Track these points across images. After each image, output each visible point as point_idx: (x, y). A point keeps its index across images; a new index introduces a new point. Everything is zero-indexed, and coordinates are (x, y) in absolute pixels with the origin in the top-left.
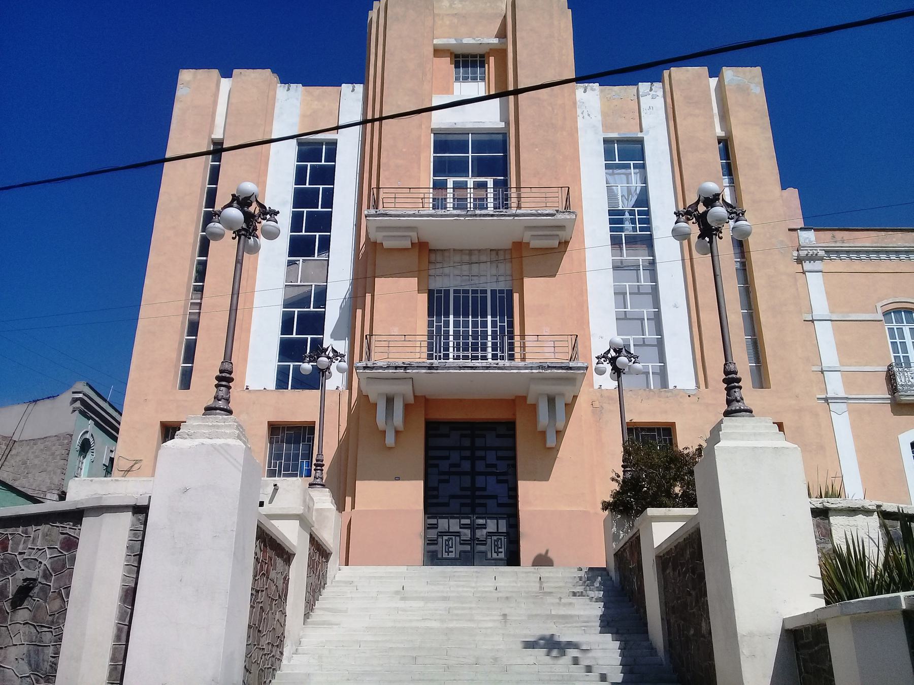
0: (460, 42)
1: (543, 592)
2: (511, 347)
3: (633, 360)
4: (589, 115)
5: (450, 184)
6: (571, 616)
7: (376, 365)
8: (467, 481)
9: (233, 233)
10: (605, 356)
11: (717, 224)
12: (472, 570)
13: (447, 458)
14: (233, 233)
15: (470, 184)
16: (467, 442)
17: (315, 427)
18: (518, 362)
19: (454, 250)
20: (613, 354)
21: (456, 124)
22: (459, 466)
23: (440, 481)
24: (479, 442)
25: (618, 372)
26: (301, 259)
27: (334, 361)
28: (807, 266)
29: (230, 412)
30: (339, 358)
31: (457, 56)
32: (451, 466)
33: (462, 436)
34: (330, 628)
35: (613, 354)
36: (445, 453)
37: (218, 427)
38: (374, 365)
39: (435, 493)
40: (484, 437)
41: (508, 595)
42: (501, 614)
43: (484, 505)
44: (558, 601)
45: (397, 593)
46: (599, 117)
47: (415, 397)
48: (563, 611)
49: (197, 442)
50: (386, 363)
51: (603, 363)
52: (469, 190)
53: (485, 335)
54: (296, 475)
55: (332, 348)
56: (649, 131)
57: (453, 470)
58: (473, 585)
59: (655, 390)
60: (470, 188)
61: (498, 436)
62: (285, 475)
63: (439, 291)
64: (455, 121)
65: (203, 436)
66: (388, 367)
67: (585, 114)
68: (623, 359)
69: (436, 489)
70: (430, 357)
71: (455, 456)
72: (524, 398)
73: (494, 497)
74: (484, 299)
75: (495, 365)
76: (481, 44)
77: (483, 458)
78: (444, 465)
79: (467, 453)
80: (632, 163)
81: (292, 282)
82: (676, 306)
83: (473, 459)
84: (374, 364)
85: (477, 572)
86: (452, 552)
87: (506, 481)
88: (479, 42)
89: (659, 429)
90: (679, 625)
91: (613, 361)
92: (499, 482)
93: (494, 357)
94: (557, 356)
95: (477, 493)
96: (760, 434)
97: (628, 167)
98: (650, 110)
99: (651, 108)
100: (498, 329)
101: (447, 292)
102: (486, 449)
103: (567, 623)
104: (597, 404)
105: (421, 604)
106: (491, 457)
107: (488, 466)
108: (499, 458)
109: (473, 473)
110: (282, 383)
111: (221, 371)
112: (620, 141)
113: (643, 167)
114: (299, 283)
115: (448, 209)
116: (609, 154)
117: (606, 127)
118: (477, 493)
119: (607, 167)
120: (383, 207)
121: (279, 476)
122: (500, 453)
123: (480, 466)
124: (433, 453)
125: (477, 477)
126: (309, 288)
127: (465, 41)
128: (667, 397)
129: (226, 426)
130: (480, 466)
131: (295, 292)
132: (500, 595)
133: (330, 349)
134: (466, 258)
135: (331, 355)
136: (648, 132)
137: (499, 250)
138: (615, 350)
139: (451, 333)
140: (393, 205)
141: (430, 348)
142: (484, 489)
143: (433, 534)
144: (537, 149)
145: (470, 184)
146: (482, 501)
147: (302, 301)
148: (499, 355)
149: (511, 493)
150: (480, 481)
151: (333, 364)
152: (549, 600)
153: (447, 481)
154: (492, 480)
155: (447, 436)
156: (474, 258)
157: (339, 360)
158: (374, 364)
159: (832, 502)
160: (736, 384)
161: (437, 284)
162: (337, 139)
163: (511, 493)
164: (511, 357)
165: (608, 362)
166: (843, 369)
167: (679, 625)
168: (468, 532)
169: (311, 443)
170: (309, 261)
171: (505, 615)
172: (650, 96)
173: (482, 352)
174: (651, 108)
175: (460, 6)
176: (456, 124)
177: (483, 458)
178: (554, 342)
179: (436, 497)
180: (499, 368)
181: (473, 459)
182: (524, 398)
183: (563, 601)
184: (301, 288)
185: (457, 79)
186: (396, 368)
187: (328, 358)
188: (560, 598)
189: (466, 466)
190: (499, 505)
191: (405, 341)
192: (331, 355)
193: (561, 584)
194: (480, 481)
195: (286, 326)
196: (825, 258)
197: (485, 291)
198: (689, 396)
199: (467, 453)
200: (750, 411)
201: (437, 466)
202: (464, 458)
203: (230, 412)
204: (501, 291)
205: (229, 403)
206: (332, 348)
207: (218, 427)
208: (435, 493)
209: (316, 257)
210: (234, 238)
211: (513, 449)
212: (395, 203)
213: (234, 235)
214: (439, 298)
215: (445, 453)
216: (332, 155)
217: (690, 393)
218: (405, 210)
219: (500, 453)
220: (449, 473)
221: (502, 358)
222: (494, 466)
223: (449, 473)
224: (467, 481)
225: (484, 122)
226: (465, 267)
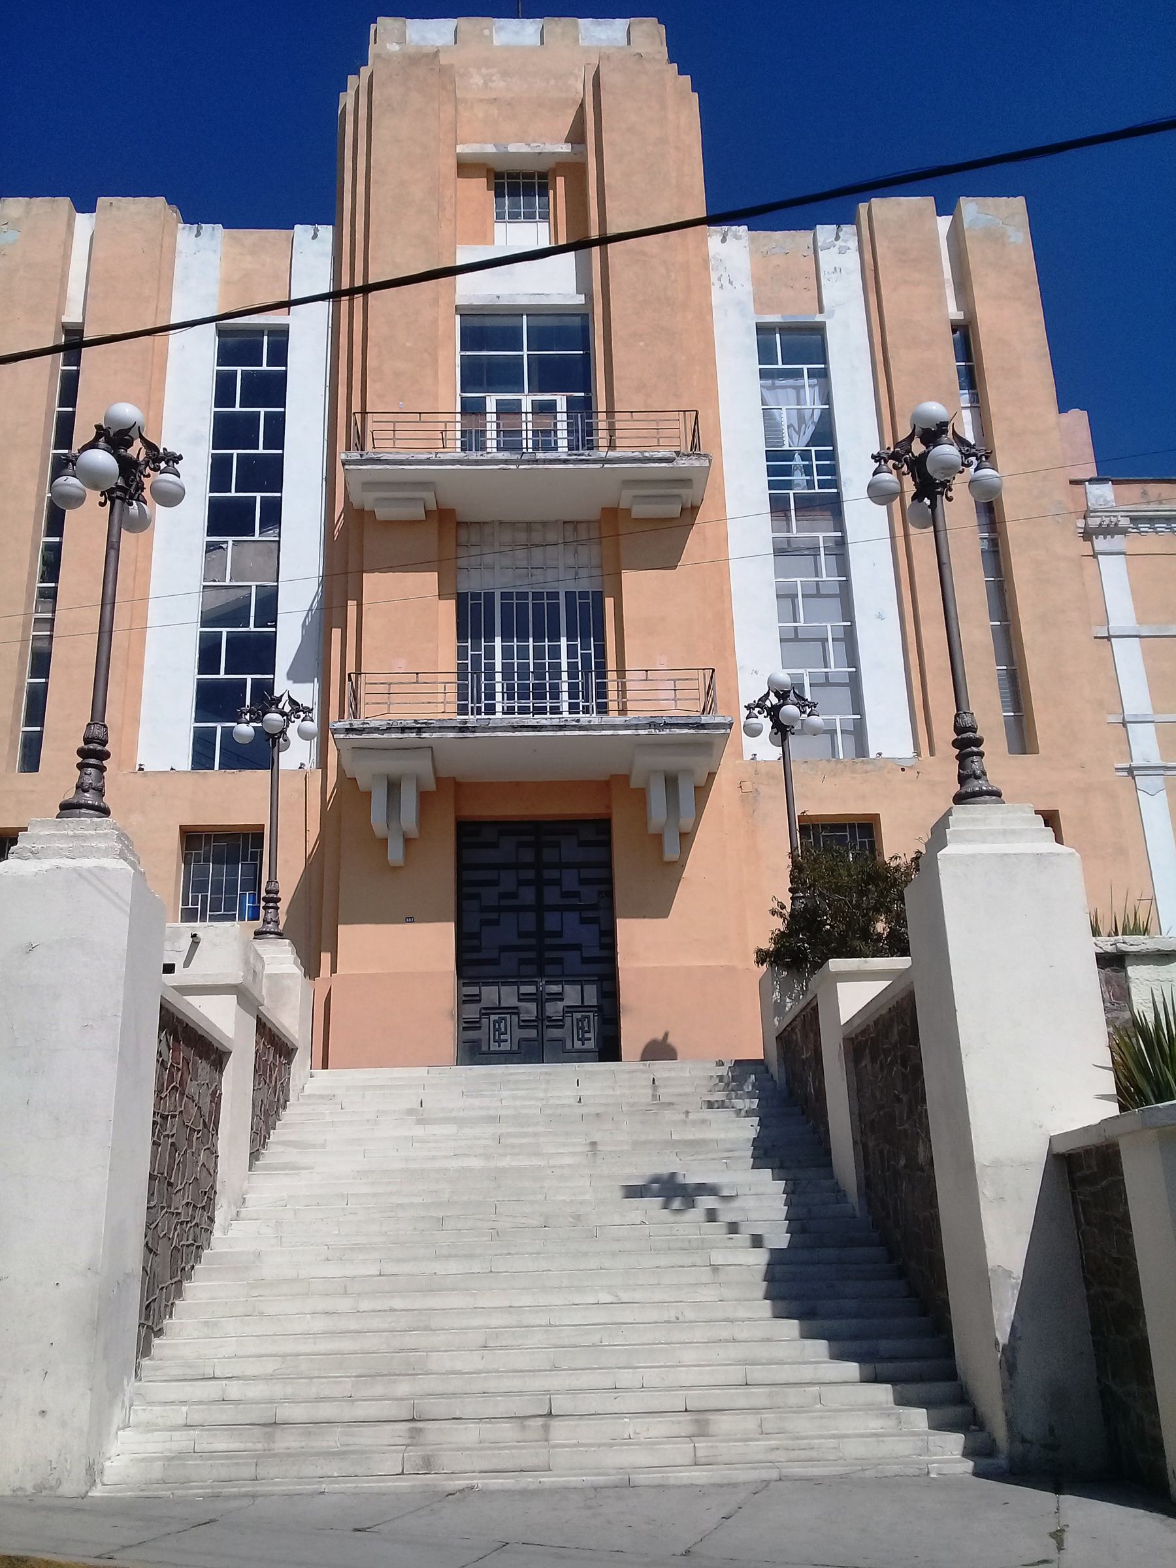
0: (502, 150)
1: (659, 1103)
2: (602, 691)
3: (808, 710)
4: (731, 283)
5: (491, 406)
6: (704, 1142)
7: (368, 726)
8: (529, 921)
9: (101, 495)
10: (760, 704)
11: (943, 475)
12: (539, 1071)
13: (495, 883)
14: (101, 495)
15: (527, 405)
16: (528, 856)
17: (263, 833)
18: (613, 717)
19: (501, 523)
20: (773, 700)
21: (498, 297)
22: (514, 895)
23: (484, 923)
24: (549, 855)
25: (782, 731)
26: (230, 539)
27: (293, 719)
28: (1101, 543)
29: (105, 812)
30: (301, 713)
31: (498, 175)
32: (504, 896)
33: (521, 845)
34: (296, 1174)
35: (773, 700)
36: (490, 875)
37: (84, 838)
38: (365, 726)
39: (475, 942)
40: (557, 845)
41: (600, 1110)
42: (588, 1141)
43: (559, 961)
44: (683, 1117)
45: (410, 1112)
46: (749, 287)
47: (438, 779)
48: (690, 1134)
49: (47, 864)
50: (385, 722)
51: (757, 717)
52: (524, 415)
53: (556, 671)
54: (232, 918)
55: (289, 696)
56: (834, 311)
57: (504, 902)
58: (541, 1095)
59: (846, 760)
60: (526, 413)
61: (583, 844)
62: (213, 918)
63: (476, 596)
64: (498, 293)
65: (58, 853)
66: (389, 729)
67: (725, 280)
68: (790, 710)
69: (477, 936)
70: (462, 710)
71: (508, 879)
72: (626, 778)
73: (577, 947)
74: (555, 608)
75: (574, 723)
76: (540, 153)
77: (557, 882)
78: (490, 895)
79: (530, 874)
80: (805, 367)
81: (214, 581)
82: (880, 617)
83: (539, 884)
84: (364, 723)
85: (546, 1073)
86: (506, 1041)
87: (595, 921)
88: (537, 151)
89: (852, 826)
90: (881, 1152)
91: (774, 713)
92: (583, 921)
93: (573, 709)
94: (680, 705)
95: (548, 941)
96: (1013, 832)
97: (798, 374)
98: (835, 275)
99: (838, 270)
100: (579, 660)
101: (490, 597)
102: (561, 866)
103: (697, 1153)
104: (748, 786)
105: (451, 1129)
106: (570, 880)
107: (565, 895)
108: (584, 882)
109: (540, 908)
110: (202, 758)
111: (87, 741)
112: (785, 329)
113: (823, 375)
114: (227, 583)
115: (489, 450)
116: (765, 353)
117: (761, 303)
118: (548, 941)
119: (763, 374)
120: (374, 448)
121: (203, 919)
122: (587, 873)
123: (552, 896)
124: (469, 875)
125: (546, 914)
126: (244, 593)
127: (513, 148)
128: (867, 772)
129: (99, 836)
130: (552, 896)
131: (221, 599)
132: (585, 1110)
133: (285, 698)
134: (522, 537)
135: (287, 709)
136: (832, 314)
137: (577, 522)
138: (777, 695)
139: (498, 668)
140: (390, 443)
141: (462, 694)
142: (559, 934)
143: (472, 1011)
144: (642, 344)
145: (527, 405)
146: (555, 954)
147: (237, 615)
148: (581, 704)
149: (606, 940)
150: (552, 921)
151: (291, 724)
152: (668, 1115)
153: (496, 922)
154: (572, 918)
155: (494, 845)
156: (537, 537)
157: (302, 718)
158: (364, 723)
159: (1132, 942)
160: (975, 749)
161: (473, 583)
162: (288, 325)
163: (606, 940)
164: (603, 709)
165: (765, 714)
166: (1158, 718)
167: (881, 1152)
168: (532, 1007)
169: (258, 863)
170: (245, 543)
171: (594, 1144)
172: (836, 249)
173: (551, 701)
174: (838, 270)
175: (502, 84)
176: (498, 297)
177: (557, 882)
178: (675, 681)
179: (477, 949)
180: (581, 728)
181: (539, 884)
182: (626, 778)
183: (691, 1116)
184: (231, 591)
185: (500, 217)
186: (403, 730)
187: (283, 714)
188: (687, 1113)
189: (528, 895)
190: (586, 961)
191: (417, 682)
192: (287, 709)
193: (688, 1090)
194: (552, 921)
195: (208, 660)
196: (1130, 530)
197: (555, 595)
198: (903, 770)
199: (530, 874)
200: (998, 794)
201: (477, 896)
202: (522, 883)
203: (105, 812)
204: (584, 595)
205: (103, 796)
206: (289, 696)
207: (84, 838)
208: (475, 942)
209: (257, 537)
210: (102, 504)
211: (608, 865)
212: (394, 439)
213: (102, 499)
214: (476, 607)
215: (490, 875)
216: (280, 354)
217: (904, 764)
218: (413, 453)
219: (587, 873)
220: (499, 909)
221: (587, 710)
222: (576, 894)
223: (499, 909)
224: (529, 921)
225: (548, 295)
226: (521, 554)
